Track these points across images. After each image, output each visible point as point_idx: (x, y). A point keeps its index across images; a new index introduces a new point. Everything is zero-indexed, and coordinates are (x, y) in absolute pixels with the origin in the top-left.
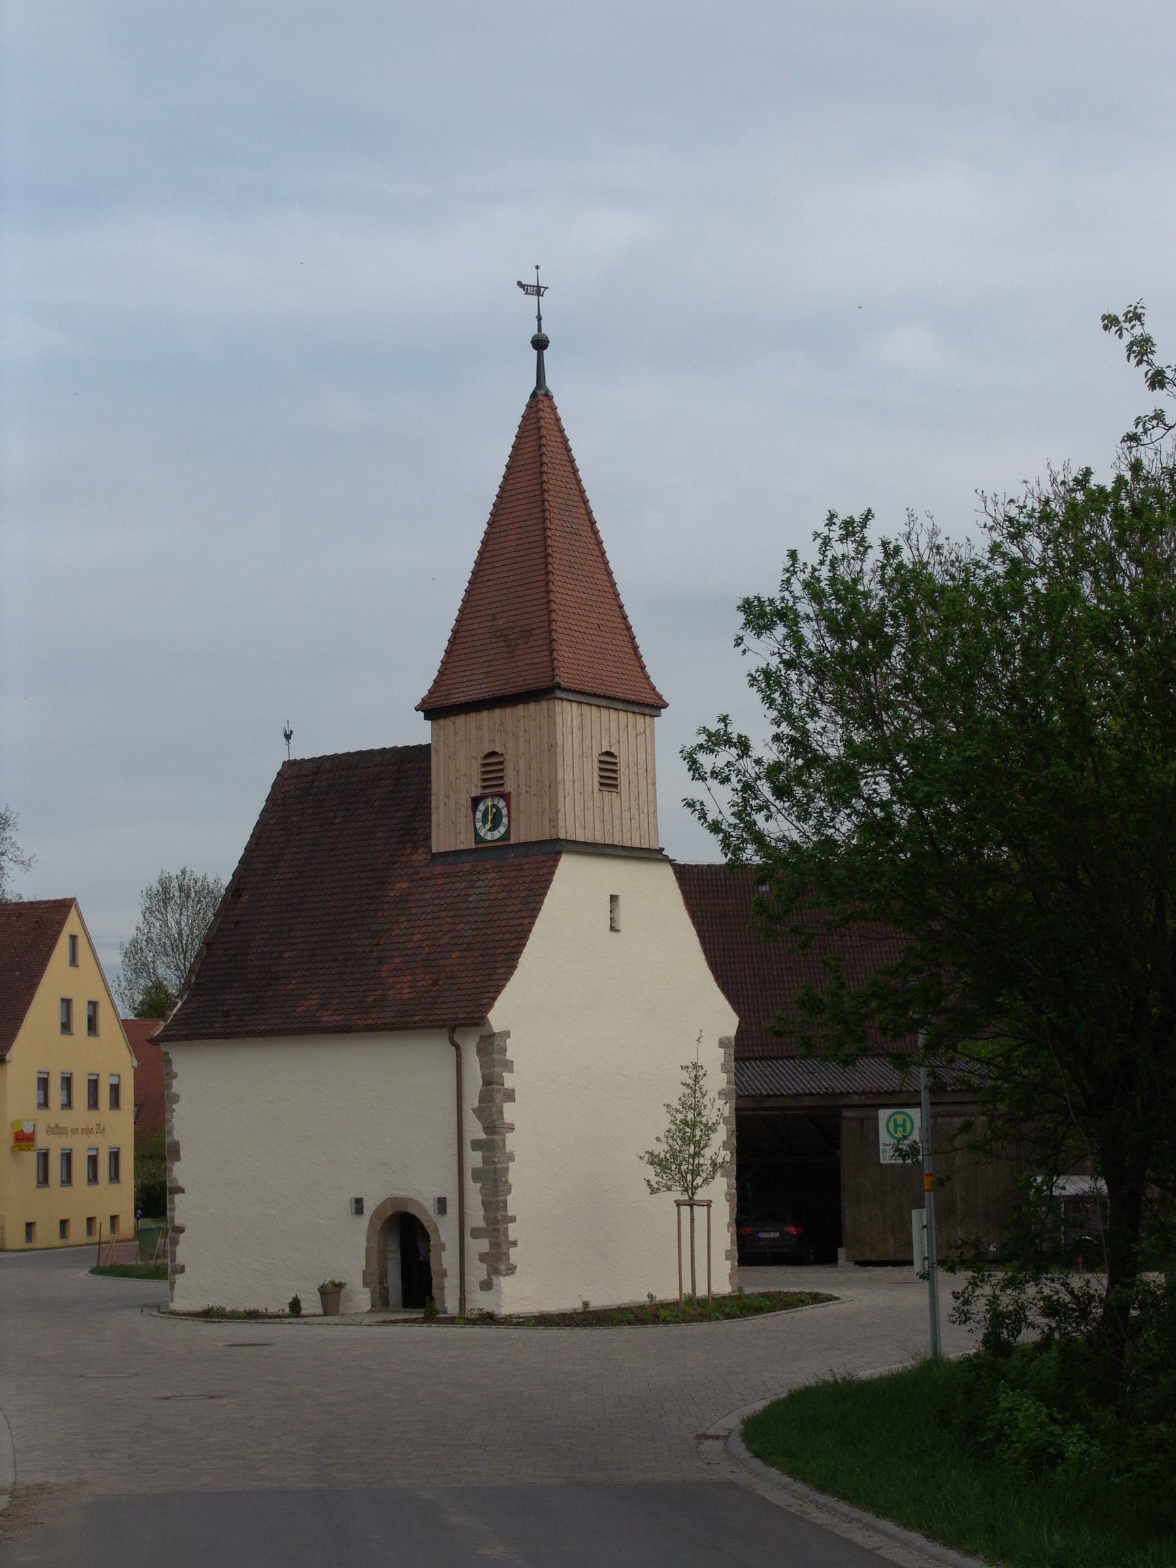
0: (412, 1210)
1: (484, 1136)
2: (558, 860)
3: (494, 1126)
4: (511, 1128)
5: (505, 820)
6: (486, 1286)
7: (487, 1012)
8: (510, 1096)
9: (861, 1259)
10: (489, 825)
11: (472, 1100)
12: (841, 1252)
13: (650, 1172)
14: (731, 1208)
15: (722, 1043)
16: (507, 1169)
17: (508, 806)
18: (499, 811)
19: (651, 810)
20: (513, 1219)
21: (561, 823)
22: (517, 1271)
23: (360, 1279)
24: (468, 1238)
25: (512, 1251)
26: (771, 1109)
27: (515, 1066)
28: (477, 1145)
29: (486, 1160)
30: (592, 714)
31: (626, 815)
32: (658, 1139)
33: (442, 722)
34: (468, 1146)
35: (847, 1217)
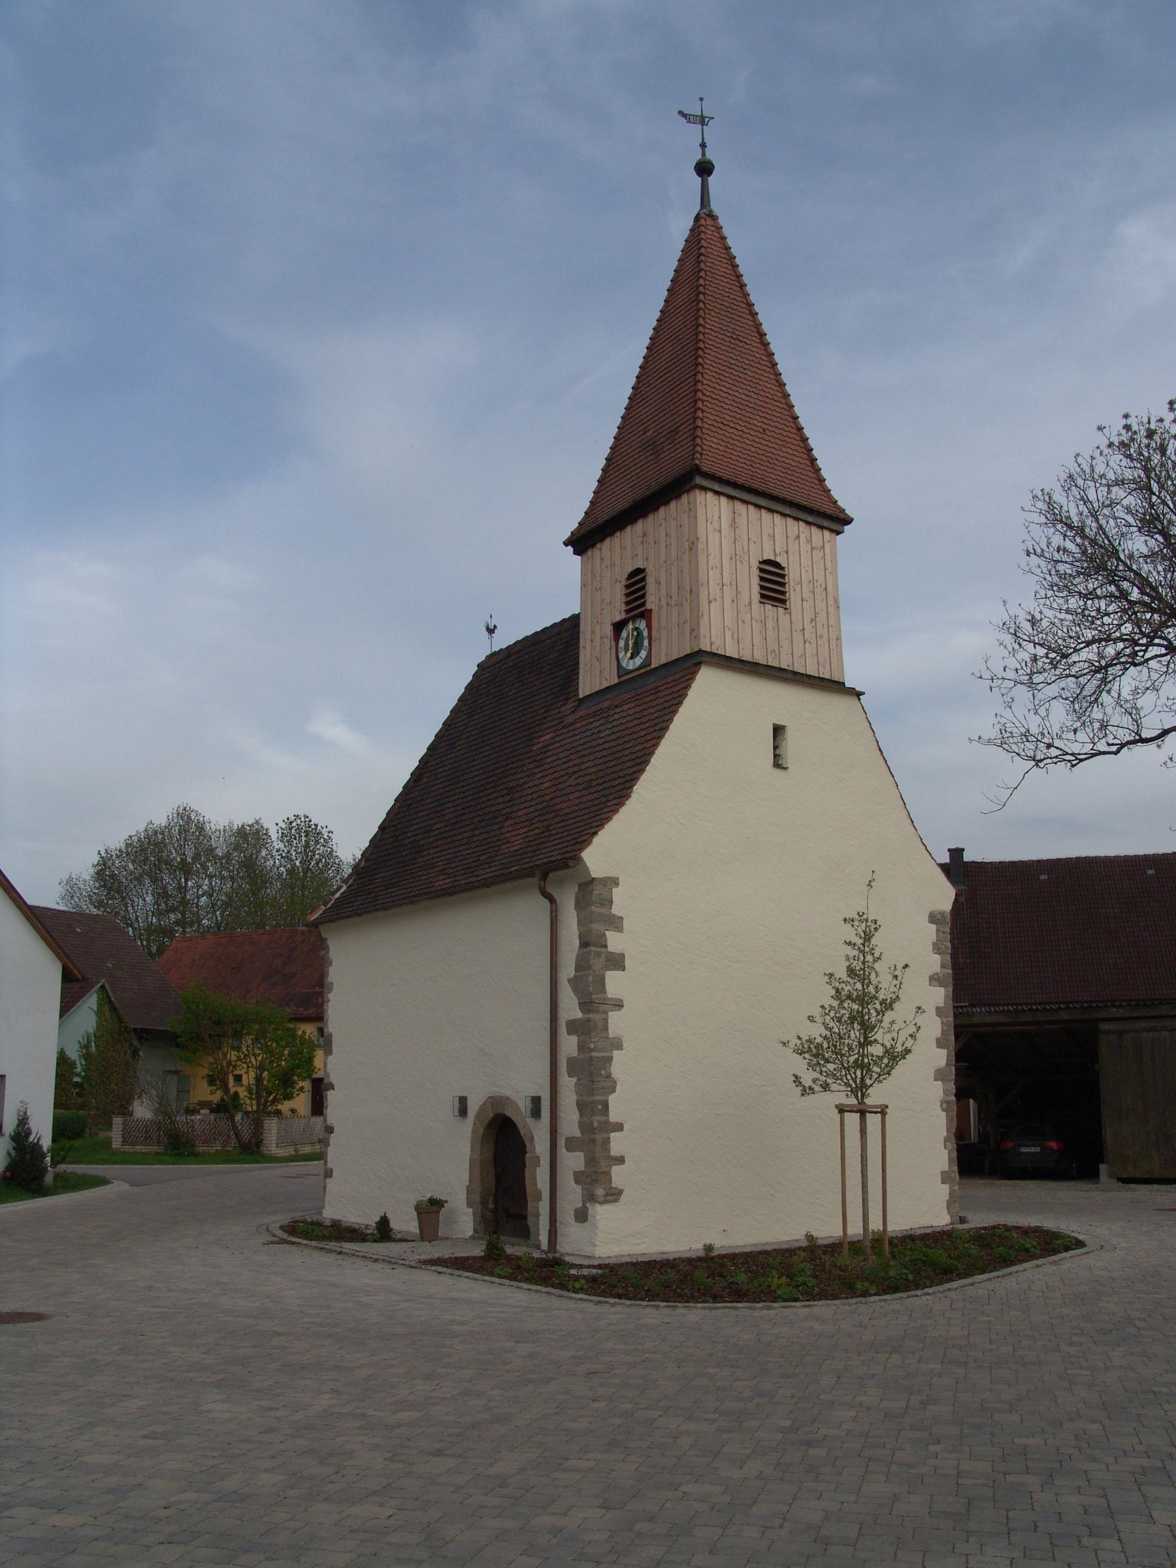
0: (509, 1113)
1: (579, 1015)
2: (696, 672)
3: (594, 1000)
4: (618, 1005)
5: (646, 643)
6: (582, 1216)
7: (582, 849)
8: (617, 962)
9: (1124, 1176)
10: (629, 655)
11: (568, 970)
12: (1103, 1168)
13: (799, 1065)
14: (949, 1120)
15: (933, 918)
16: (610, 1059)
17: (649, 626)
18: (640, 633)
19: (833, 636)
20: (619, 1127)
21: (703, 631)
22: (623, 1198)
23: (463, 1196)
24: (562, 1151)
25: (616, 1170)
26: (1023, 1024)
27: (626, 924)
28: (573, 1027)
29: (582, 1047)
30: (749, 516)
31: (797, 637)
32: (811, 1018)
33: (589, 552)
34: (563, 1030)
35: (1108, 1135)
